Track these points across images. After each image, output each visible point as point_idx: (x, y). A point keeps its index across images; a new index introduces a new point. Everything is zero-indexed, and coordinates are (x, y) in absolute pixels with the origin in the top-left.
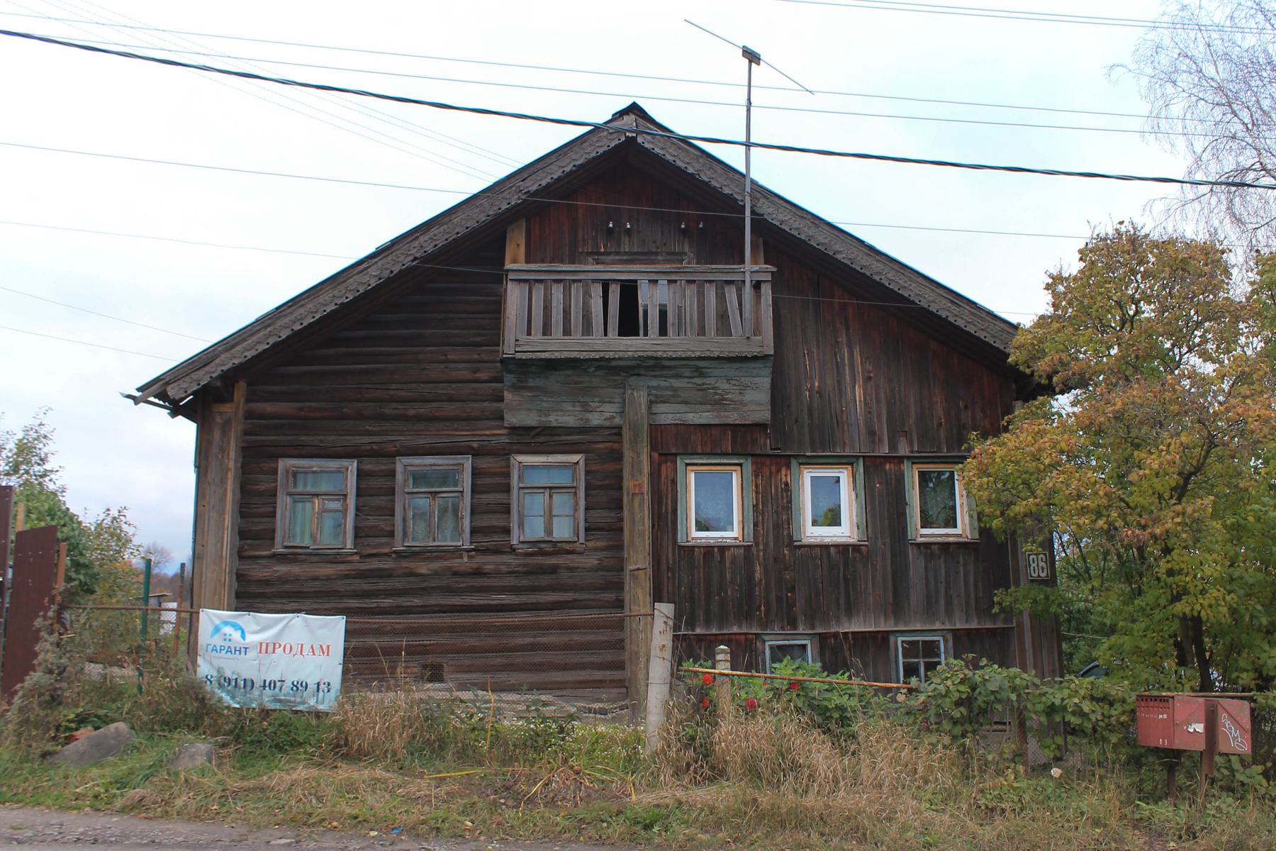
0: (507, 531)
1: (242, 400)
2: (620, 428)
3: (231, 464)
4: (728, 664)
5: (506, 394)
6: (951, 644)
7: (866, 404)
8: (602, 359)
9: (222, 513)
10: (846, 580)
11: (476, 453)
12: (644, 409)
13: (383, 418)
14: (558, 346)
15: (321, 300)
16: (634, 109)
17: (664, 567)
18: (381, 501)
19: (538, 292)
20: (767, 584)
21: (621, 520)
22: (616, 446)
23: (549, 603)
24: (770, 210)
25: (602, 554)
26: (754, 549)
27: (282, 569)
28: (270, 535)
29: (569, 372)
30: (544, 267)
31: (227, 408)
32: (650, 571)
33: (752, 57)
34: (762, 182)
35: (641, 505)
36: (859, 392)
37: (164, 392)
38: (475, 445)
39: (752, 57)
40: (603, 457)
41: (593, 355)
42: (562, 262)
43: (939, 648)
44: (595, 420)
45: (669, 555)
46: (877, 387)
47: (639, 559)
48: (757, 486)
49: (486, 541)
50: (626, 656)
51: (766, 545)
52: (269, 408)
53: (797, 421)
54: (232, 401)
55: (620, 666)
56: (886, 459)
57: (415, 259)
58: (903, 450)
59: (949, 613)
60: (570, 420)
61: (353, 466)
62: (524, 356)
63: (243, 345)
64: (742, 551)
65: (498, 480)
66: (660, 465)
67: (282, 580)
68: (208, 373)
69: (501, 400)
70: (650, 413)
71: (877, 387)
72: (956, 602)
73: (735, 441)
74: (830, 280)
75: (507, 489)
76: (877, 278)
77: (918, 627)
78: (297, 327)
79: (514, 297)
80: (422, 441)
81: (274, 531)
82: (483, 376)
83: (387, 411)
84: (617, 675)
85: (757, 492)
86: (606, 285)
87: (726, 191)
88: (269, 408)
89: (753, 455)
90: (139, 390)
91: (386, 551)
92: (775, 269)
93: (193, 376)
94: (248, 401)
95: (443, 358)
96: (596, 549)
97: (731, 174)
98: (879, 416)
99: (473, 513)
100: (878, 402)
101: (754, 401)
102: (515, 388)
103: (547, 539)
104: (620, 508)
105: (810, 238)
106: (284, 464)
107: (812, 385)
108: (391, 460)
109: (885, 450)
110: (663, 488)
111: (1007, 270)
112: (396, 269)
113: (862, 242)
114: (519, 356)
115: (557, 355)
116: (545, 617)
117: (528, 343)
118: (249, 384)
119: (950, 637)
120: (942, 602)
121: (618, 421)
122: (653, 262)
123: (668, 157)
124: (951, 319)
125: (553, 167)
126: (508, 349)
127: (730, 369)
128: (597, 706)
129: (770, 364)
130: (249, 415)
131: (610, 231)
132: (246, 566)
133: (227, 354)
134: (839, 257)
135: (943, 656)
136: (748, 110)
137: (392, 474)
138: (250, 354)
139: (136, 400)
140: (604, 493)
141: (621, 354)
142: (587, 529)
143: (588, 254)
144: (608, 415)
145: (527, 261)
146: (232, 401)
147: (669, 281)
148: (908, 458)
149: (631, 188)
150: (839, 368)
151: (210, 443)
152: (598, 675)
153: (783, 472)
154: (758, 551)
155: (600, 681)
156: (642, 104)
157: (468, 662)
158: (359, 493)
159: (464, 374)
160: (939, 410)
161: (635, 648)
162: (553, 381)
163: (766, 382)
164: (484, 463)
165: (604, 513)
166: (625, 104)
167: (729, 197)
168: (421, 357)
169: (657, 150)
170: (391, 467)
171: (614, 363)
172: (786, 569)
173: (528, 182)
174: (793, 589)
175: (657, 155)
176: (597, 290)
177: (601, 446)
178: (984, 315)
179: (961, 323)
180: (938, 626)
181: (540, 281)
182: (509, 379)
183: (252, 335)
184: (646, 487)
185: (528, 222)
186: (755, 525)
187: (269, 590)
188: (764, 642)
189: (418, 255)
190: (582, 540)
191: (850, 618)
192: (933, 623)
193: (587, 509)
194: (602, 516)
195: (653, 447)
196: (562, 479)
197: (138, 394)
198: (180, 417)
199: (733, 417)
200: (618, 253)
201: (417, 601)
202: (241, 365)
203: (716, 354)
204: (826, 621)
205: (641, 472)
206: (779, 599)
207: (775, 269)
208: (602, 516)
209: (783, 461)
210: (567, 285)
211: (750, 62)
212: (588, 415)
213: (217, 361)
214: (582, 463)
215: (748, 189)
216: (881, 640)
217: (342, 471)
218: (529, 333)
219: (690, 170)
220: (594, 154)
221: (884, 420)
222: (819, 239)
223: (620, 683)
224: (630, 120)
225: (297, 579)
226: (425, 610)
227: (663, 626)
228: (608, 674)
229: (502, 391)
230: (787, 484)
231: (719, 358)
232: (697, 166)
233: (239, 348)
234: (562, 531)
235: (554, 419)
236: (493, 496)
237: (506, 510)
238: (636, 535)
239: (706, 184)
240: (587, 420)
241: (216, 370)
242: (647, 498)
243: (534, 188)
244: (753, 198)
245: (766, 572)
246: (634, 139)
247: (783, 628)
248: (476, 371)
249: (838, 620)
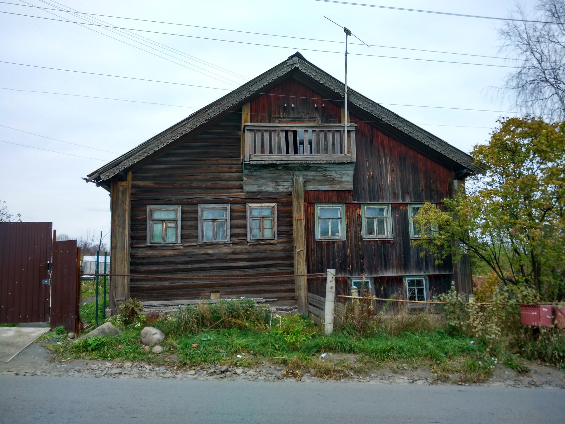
0: (245, 235)
1: (130, 181)
2: (291, 192)
3: (127, 208)
4: (357, 294)
5: (244, 178)
6: (428, 281)
7: (392, 181)
8: (286, 164)
9: (124, 229)
10: (384, 255)
11: (232, 203)
12: (302, 185)
13: (192, 188)
14: (267, 158)
15: (166, 137)
16: (298, 55)
17: (310, 250)
18: (192, 223)
19: (259, 135)
20: (352, 257)
21: (292, 230)
22: (290, 200)
23: (263, 265)
24: (355, 100)
25: (285, 244)
26: (346, 242)
27: (150, 252)
28: (144, 238)
29: (271, 169)
30: (262, 124)
31: (124, 183)
32: (305, 251)
33: (348, 32)
34: (351, 87)
35: (301, 225)
36: (389, 176)
37: (98, 178)
38: (231, 199)
39: (348, 32)
40: (284, 204)
41: (282, 162)
42: (265, 122)
43: (423, 282)
44: (281, 189)
45: (313, 245)
46: (397, 174)
47: (300, 247)
48: (347, 216)
49: (237, 239)
50: (296, 287)
51: (351, 240)
52: (141, 183)
53: (363, 189)
54: (127, 180)
55: (293, 291)
56: (401, 204)
57: (206, 120)
58: (408, 200)
59: (427, 268)
60: (270, 189)
61: (179, 208)
62: (253, 163)
63: (133, 157)
64: (342, 243)
65: (242, 214)
66: (308, 207)
67: (149, 257)
68: (118, 169)
69: (242, 180)
70: (304, 186)
71: (397, 174)
72: (429, 263)
73: (339, 197)
74: (381, 131)
75: (245, 218)
76: (400, 129)
77: (415, 274)
78: (156, 149)
79: (248, 137)
80: (208, 197)
81: (146, 236)
82: (234, 170)
83: (194, 185)
84: (292, 294)
85: (347, 219)
86: (287, 132)
87: (337, 91)
88: (141, 183)
89: (345, 203)
90: (88, 176)
91: (195, 244)
92: (356, 125)
93: (111, 170)
94: (132, 180)
95: (216, 162)
96: (281, 243)
97: (339, 84)
98: (397, 186)
99: (231, 228)
100: (397, 180)
101: (346, 180)
102: (248, 176)
103: (262, 238)
104: (291, 225)
105: (372, 111)
106: (149, 208)
107: (370, 173)
108: (196, 206)
109: (400, 201)
110: (309, 217)
111: (465, 130)
112: (198, 124)
113: (393, 113)
114: (251, 162)
115: (267, 162)
116: (262, 271)
117: (255, 157)
118: (132, 173)
119: (427, 278)
120: (424, 263)
121: (290, 189)
122: (304, 122)
123: (312, 76)
124: (430, 146)
125: (264, 80)
126: (247, 160)
127: (337, 168)
128: (284, 308)
129: (354, 165)
130: (133, 187)
131: (285, 108)
132: (134, 251)
133: (126, 161)
134: (384, 120)
135: (424, 286)
136: (346, 55)
137: (196, 212)
138: (136, 161)
139: (87, 181)
140: (285, 219)
141: (293, 162)
142: (278, 234)
143: (276, 118)
144: (286, 187)
145: (251, 122)
146: (127, 180)
147: (313, 131)
148: (410, 204)
149: (296, 90)
150: (381, 166)
151: (117, 198)
152: (284, 295)
153: (358, 210)
154: (348, 243)
155: (285, 297)
156: (302, 52)
157: (230, 290)
158: (183, 220)
159: (226, 170)
160: (422, 183)
161: (299, 283)
162: (264, 173)
163: (352, 173)
164: (235, 207)
165: (286, 228)
166: (293, 52)
167: (338, 93)
168: (207, 162)
169: (307, 73)
170: (196, 209)
171: (290, 165)
172: (360, 250)
173: (254, 87)
174: (362, 258)
175: (307, 75)
176: (283, 135)
177: (283, 200)
178: (444, 144)
179: (434, 148)
180: (422, 273)
181: (259, 131)
182: (246, 172)
183: (137, 152)
184: (303, 217)
185: (251, 103)
186: (347, 232)
187: (145, 261)
188: (351, 280)
189: (208, 118)
190: (276, 238)
191: (386, 271)
192: (420, 272)
193: (278, 226)
194: (284, 229)
195: (305, 201)
196: (266, 213)
197: (88, 178)
198: (100, 187)
199: (337, 187)
200: (288, 118)
201: (208, 265)
202: (132, 165)
203: (332, 162)
204: (377, 272)
205: (300, 210)
206: (357, 263)
207: (356, 125)
208: (284, 229)
209: (358, 206)
210: (270, 132)
211: (347, 34)
212: (278, 187)
213: (122, 163)
214: (276, 207)
215: (346, 90)
216: (399, 280)
217: (176, 211)
218: (255, 153)
219: (321, 82)
220: (281, 75)
221: (400, 188)
222: (375, 112)
223: (293, 298)
224: (296, 59)
225: (157, 257)
226: (212, 269)
227: (332, 279)
228: (287, 294)
229: (242, 177)
230: (359, 215)
231: (334, 163)
232: (324, 80)
233: (131, 158)
234: (268, 234)
235: (264, 189)
236: (239, 220)
237: (245, 226)
238: (299, 236)
239: (328, 88)
240: (278, 189)
241: (121, 167)
242: (303, 222)
243: (256, 89)
244: (348, 95)
245: (351, 252)
246: (298, 68)
247: (359, 275)
248: (231, 168)
249: (382, 271)
